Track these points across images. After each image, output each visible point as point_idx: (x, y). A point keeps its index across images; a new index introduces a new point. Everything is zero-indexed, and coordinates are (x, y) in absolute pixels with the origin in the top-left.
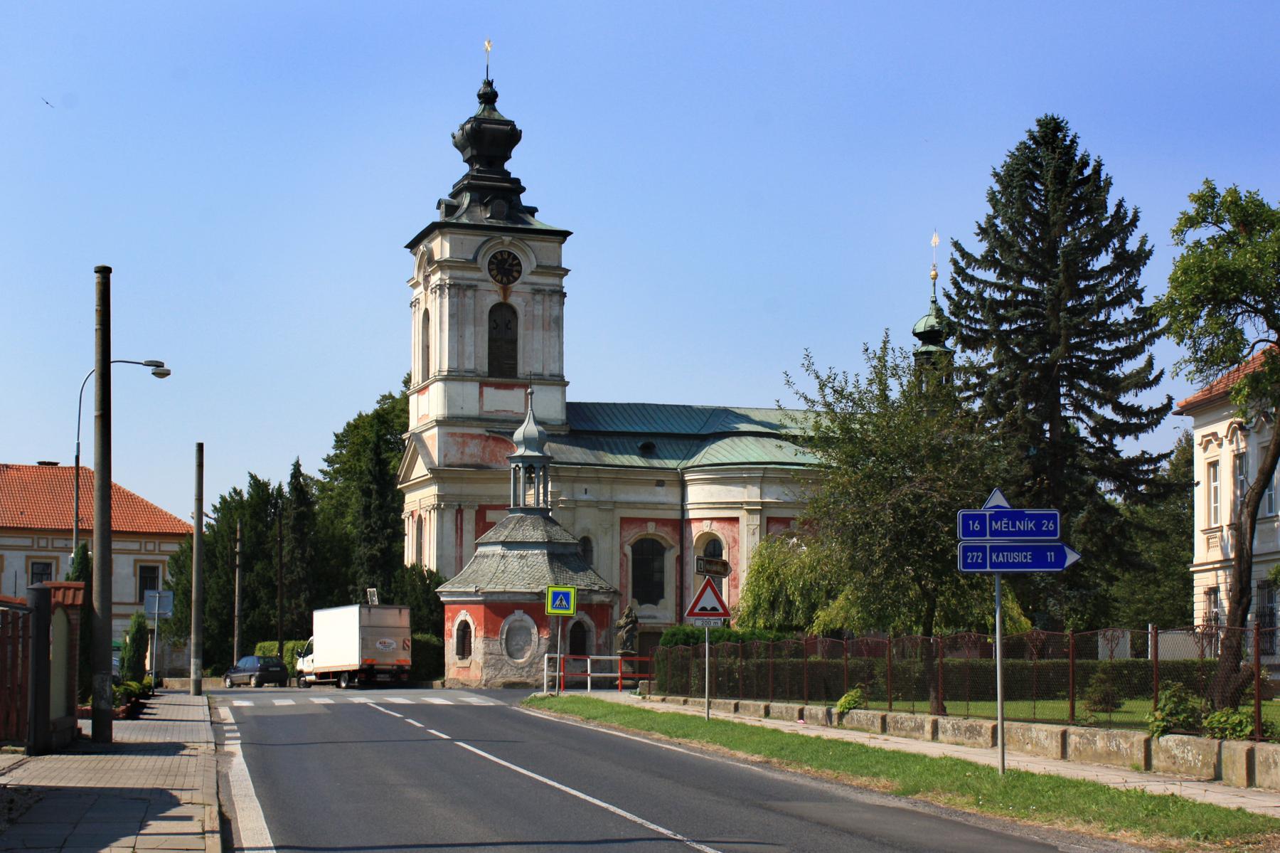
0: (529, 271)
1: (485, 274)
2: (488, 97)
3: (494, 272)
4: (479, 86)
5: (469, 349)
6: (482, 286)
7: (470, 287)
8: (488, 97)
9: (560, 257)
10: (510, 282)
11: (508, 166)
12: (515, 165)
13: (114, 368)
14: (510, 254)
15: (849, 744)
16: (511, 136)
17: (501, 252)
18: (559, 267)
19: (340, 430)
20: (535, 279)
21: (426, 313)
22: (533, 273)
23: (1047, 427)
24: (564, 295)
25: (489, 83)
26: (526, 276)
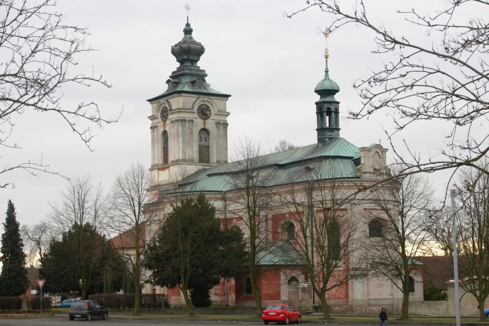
0: (214, 114)
1: (196, 115)
2: (188, 31)
3: (200, 114)
4: (184, 27)
5: (156, 155)
6: (195, 120)
7: (155, 126)
8: (188, 31)
9: (225, 107)
10: (206, 119)
11: (199, 64)
12: (202, 63)
13: (460, 59)
14: (206, 105)
15: (458, 265)
16: (200, 51)
17: (202, 105)
18: (225, 112)
19: (7, 212)
20: (216, 118)
21: (165, 133)
22: (216, 115)
23: (81, 280)
24: (227, 124)
25: (188, 25)
26: (212, 117)
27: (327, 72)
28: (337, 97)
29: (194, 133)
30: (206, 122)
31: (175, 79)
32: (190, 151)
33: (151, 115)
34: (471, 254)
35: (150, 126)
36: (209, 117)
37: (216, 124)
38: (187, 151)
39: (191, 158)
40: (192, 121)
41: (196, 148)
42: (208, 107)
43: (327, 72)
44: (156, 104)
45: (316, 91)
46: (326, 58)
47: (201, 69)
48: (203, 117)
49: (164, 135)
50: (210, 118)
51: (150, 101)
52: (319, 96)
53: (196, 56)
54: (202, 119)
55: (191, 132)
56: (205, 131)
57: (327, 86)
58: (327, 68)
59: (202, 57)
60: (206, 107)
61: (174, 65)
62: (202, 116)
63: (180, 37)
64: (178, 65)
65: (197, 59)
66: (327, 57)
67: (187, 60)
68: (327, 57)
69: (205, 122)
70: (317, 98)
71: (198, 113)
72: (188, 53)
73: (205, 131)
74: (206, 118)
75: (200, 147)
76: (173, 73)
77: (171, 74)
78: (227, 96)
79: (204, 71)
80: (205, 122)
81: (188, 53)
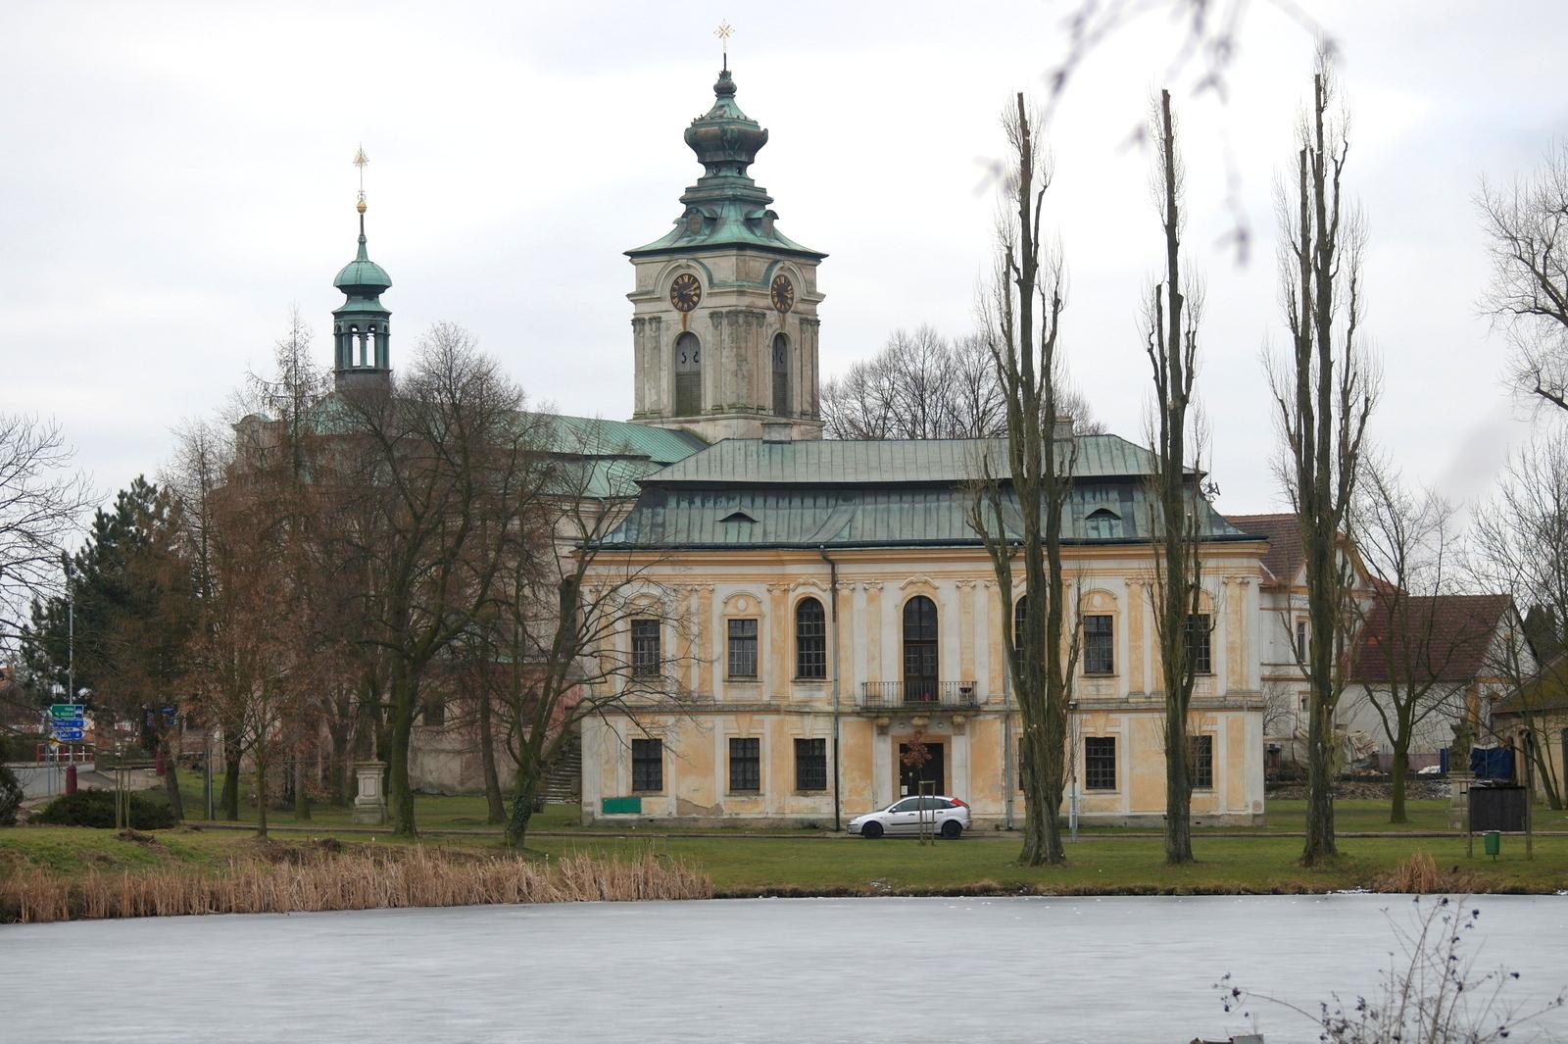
1: (667, 305)
2: (725, 89)
6: (664, 316)
8: (725, 89)
10: (690, 309)
11: (751, 171)
12: (761, 171)
24: (818, 322)
25: (725, 75)
27: (362, 242)
28: (385, 300)
29: (664, 348)
30: (689, 317)
31: (699, 205)
32: (653, 391)
33: (633, 289)
34: (533, 697)
35: (633, 317)
36: (695, 304)
37: (801, 324)
38: (647, 392)
39: (654, 408)
40: (658, 320)
41: (666, 382)
42: (789, 284)
43: (362, 242)
44: (662, 265)
45: (343, 288)
46: (360, 211)
47: (757, 185)
48: (683, 306)
49: (678, 344)
50: (699, 306)
51: (634, 255)
52: (345, 296)
53: (721, 153)
54: (681, 309)
55: (654, 345)
56: (686, 338)
57: (368, 278)
58: (362, 234)
59: (759, 155)
60: (689, 279)
61: (691, 170)
62: (680, 304)
63: (705, 102)
64: (701, 171)
65: (743, 158)
66: (362, 210)
67: (728, 164)
68: (362, 210)
69: (685, 317)
70: (340, 300)
71: (672, 298)
72: (726, 144)
73: (686, 338)
74: (688, 305)
75: (679, 378)
76: (688, 190)
77: (683, 193)
78: (817, 257)
79: (764, 190)
80: (685, 317)
81: (726, 144)
